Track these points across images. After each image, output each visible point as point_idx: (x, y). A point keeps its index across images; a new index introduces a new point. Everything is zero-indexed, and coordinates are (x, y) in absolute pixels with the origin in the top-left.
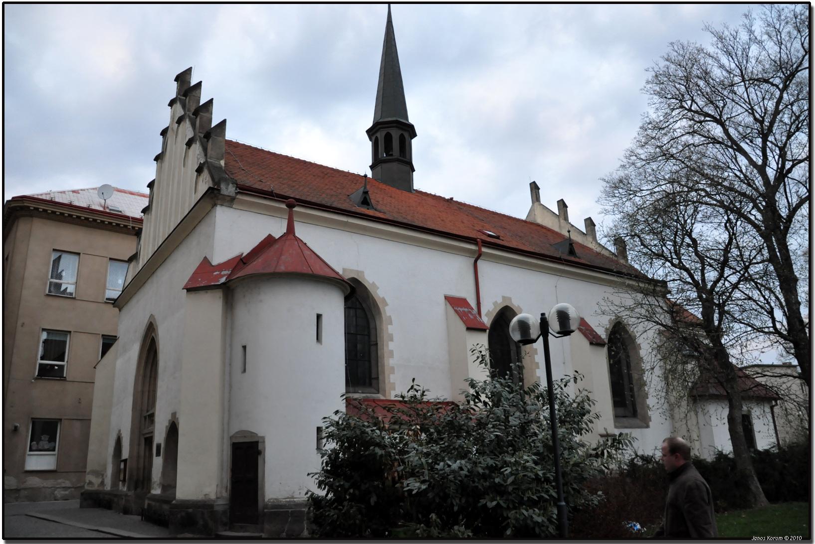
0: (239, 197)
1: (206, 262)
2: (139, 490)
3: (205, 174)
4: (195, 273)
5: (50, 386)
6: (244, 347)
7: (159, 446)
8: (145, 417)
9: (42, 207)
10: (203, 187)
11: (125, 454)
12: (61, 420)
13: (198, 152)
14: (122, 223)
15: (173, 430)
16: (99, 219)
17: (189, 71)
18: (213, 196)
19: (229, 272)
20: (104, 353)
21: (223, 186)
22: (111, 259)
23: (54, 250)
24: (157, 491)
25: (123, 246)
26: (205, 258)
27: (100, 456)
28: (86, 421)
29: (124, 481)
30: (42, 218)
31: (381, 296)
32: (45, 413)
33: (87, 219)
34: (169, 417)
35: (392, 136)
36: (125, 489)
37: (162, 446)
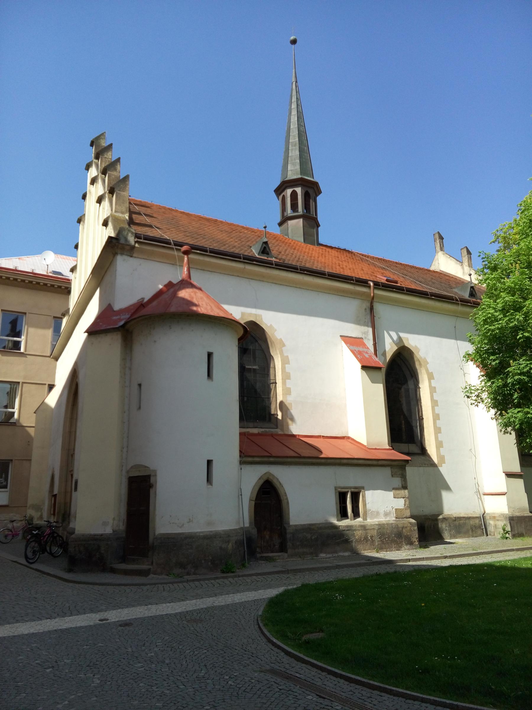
6: (140, 385)
11: (56, 492)
22: (54, 317)
31: (279, 338)
35: (302, 195)
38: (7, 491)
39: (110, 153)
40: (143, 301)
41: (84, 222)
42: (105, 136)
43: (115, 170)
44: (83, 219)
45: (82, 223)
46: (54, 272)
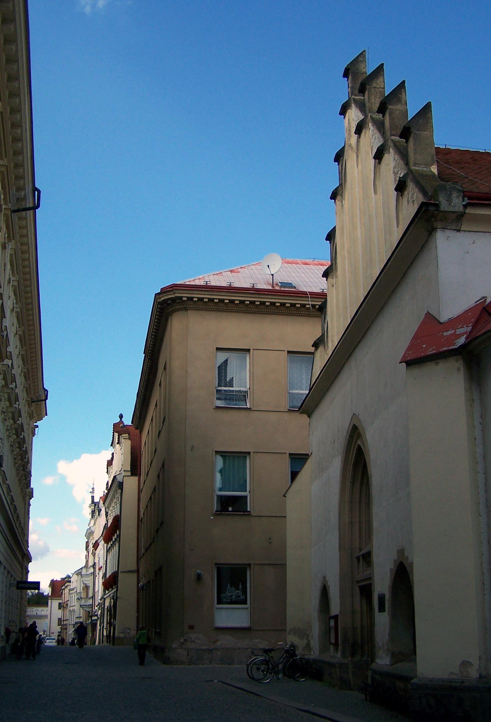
0: (469, 210)
1: (430, 319)
2: (358, 657)
3: (411, 188)
4: (416, 337)
5: (233, 523)
7: (382, 598)
8: (358, 558)
9: (196, 296)
10: (409, 210)
11: (335, 609)
12: (249, 565)
13: (392, 164)
14: (299, 302)
15: (402, 575)
16: (268, 300)
17: (361, 57)
18: (427, 221)
19: (469, 329)
20: (294, 475)
21: (442, 200)
22: (289, 352)
23: (218, 349)
24: (383, 661)
25: (301, 333)
26: (428, 314)
27: (302, 606)
28: (281, 566)
29: (336, 645)
30: (198, 309)
32: (231, 558)
33: (252, 303)
34: (394, 556)
36: (339, 655)
37: (387, 597)
38: (247, 608)
39: (381, 79)
40: (485, 301)
41: (342, 196)
42: (365, 56)
43: (399, 101)
44: (340, 192)
45: (339, 198)
46: (283, 284)
